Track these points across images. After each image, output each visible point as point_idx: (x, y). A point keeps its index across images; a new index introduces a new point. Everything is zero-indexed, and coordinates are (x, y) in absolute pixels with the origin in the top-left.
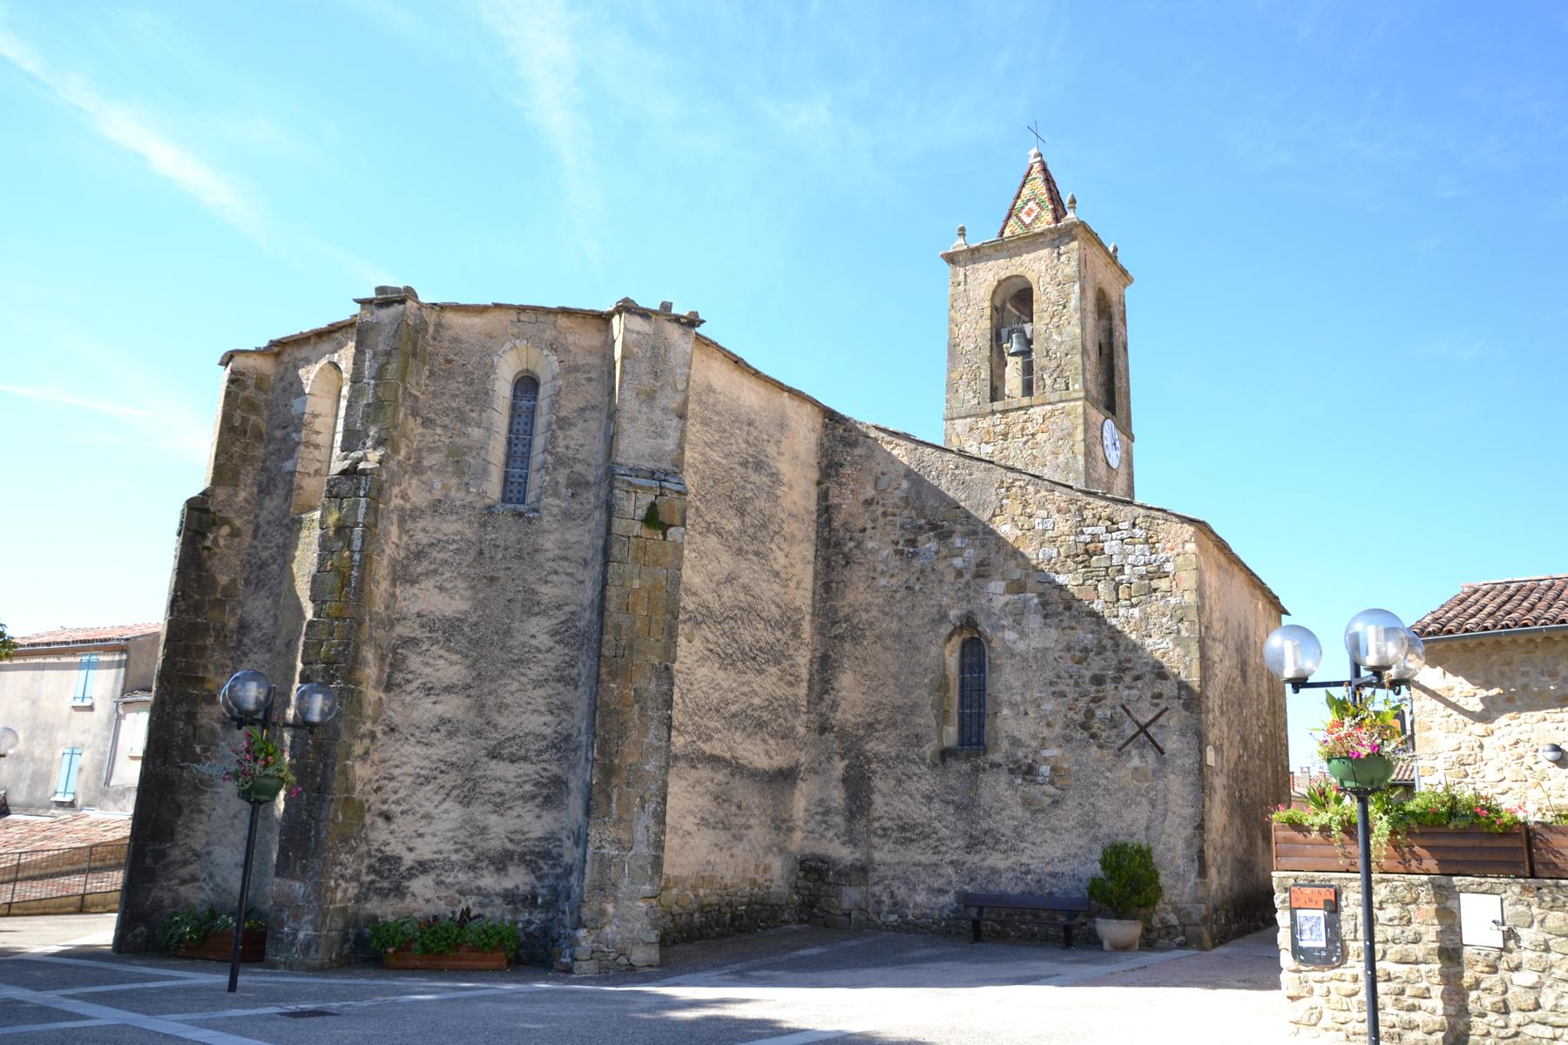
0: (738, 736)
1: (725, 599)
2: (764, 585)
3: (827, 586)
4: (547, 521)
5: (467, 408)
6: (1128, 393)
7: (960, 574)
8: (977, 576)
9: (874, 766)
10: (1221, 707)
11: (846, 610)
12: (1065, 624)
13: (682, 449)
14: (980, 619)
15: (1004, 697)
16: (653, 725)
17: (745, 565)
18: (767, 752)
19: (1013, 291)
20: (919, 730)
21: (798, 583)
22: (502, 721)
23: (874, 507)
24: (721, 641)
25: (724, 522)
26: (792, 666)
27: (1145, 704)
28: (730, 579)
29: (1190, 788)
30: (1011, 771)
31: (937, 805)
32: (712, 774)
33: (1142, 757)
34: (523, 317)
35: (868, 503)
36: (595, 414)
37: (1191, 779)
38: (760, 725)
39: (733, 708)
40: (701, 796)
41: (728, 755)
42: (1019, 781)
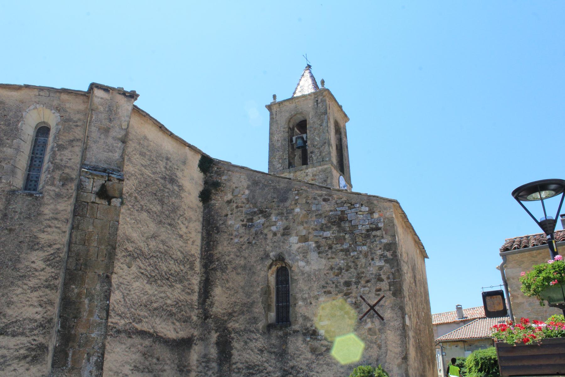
0: (158, 320)
1: (151, 246)
2: (174, 241)
3: (208, 244)
4: (47, 199)
5: (5, 138)
6: (349, 167)
7: (275, 234)
8: (283, 235)
9: (232, 335)
10: (409, 296)
11: (218, 255)
12: (330, 256)
13: (123, 159)
14: (286, 257)
15: (299, 295)
16: (97, 312)
17: (163, 230)
18: (175, 329)
19: (298, 121)
20: (256, 315)
21: (193, 242)
22: (9, 312)
23: (232, 204)
24: (148, 268)
25: (151, 206)
26: (190, 284)
27: (372, 295)
28: (154, 237)
29: (398, 337)
30: (304, 334)
31: (266, 354)
32: (141, 341)
33: (372, 322)
34: (41, 93)
35: (229, 202)
36: (79, 143)
37: (399, 332)
38: (171, 314)
39: (155, 305)
40: (135, 353)
41: (152, 331)
42: (308, 339)
